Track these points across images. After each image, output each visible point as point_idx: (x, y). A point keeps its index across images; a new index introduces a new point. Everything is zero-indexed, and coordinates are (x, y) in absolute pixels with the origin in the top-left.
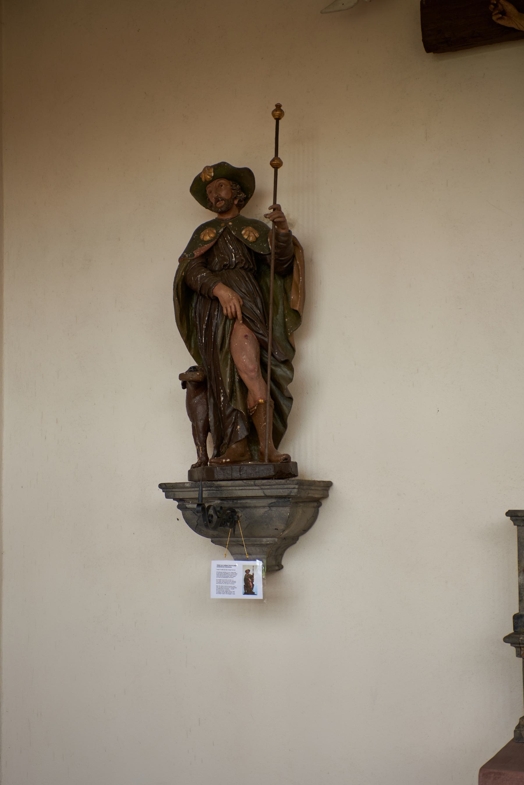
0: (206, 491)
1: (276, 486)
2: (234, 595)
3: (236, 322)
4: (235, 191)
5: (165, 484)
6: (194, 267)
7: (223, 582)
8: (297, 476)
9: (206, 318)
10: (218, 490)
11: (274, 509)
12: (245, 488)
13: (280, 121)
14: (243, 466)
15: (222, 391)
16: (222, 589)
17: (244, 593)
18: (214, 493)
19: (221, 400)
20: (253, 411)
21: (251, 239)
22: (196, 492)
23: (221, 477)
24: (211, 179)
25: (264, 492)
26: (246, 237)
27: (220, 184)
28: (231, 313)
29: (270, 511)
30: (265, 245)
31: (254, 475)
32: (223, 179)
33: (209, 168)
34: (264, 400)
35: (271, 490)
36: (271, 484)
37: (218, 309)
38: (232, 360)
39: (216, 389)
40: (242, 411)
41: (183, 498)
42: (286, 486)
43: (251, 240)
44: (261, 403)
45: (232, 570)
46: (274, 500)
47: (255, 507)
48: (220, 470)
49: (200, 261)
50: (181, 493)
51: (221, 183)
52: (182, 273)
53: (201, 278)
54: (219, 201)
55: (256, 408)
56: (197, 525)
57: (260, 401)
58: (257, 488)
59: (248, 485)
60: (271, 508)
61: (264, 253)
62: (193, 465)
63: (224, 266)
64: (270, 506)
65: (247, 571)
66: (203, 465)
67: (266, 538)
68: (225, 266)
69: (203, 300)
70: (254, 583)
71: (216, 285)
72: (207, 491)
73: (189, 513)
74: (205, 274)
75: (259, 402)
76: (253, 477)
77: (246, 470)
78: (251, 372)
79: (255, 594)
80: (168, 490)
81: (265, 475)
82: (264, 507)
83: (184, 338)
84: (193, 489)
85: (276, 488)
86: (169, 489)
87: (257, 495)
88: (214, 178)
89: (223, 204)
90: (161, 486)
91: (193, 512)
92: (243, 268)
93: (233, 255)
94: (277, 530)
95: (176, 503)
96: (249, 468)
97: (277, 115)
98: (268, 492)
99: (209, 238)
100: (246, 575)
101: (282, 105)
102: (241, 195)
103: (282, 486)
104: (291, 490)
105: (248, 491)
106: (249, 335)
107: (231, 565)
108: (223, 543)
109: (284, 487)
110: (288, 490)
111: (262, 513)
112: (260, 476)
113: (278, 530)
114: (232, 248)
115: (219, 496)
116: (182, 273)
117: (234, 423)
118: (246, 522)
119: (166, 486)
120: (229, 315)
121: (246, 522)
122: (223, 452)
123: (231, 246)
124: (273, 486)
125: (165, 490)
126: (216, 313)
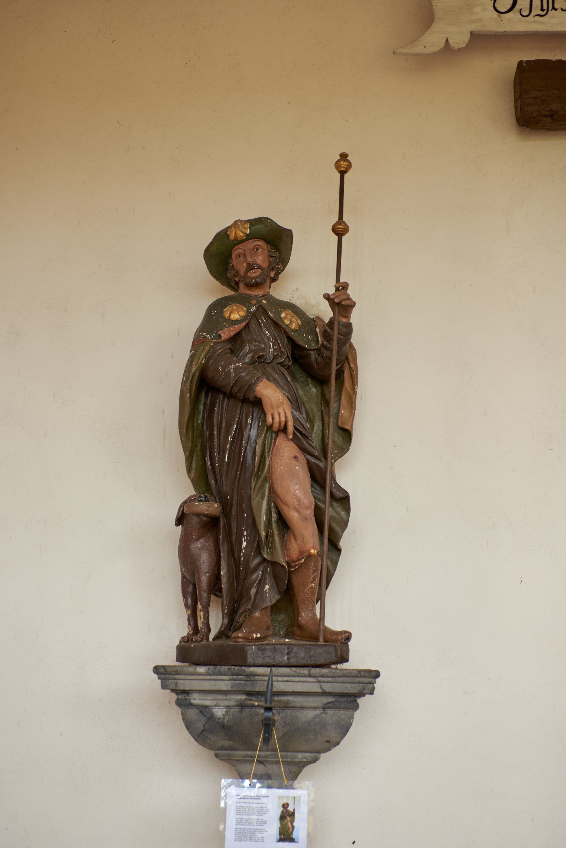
0: (230, 680)
1: (342, 679)
2: (262, 842)
3: (279, 436)
4: (273, 259)
5: (163, 667)
6: (220, 353)
7: (246, 822)
8: (347, 661)
9: (233, 426)
10: (248, 679)
11: (330, 712)
12: (294, 679)
13: (346, 176)
14: (292, 646)
15: (245, 533)
16: (244, 834)
17: (278, 840)
18: (241, 684)
19: (241, 547)
20: (296, 565)
21: (294, 326)
22: (213, 681)
23: (259, 661)
24: (244, 238)
25: (321, 686)
26: (287, 322)
27: (255, 246)
28: (279, 423)
29: (323, 715)
30: (310, 337)
31: (307, 660)
32: (260, 240)
33: (243, 222)
34: (317, 551)
35: (334, 684)
36: (336, 675)
37: (253, 415)
38: (272, 490)
39: (235, 529)
40: (285, 565)
41: (190, 689)
42: (356, 680)
43: (294, 327)
44: (313, 555)
45: (261, 803)
46: (330, 699)
47: (302, 708)
48: (257, 650)
49: (228, 347)
50: (187, 682)
51: (257, 245)
52: (202, 360)
53: (236, 369)
54: (253, 268)
55: (303, 561)
56: (203, 731)
57: (312, 551)
58: (312, 679)
59: (299, 675)
60: (325, 710)
61: (309, 348)
62: (183, 638)
63: (258, 357)
64: (325, 707)
65: (285, 806)
66: (205, 639)
67: (304, 754)
68: (260, 357)
69: (226, 400)
70: (294, 824)
71: (261, 381)
72: (230, 682)
73: (192, 713)
74: (240, 364)
75: (310, 552)
76: (306, 663)
77: (296, 653)
78: (307, 509)
79: (296, 840)
80: (167, 676)
81: (323, 661)
82: (315, 708)
83: (187, 453)
84: (209, 677)
85: (342, 682)
86: (169, 676)
87: (311, 691)
88: (249, 237)
89: (258, 274)
90: (157, 670)
91: (201, 711)
92: (281, 364)
93: (271, 344)
94: (328, 743)
95: (174, 696)
96: (300, 649)
97: (344, 166)
98: (328, 687)
99: (239, 317)
100: (283, 810)
101: (348, 155)
102: (280, 266)
103: (351, 678)
104: (364, 686)
105: (296, 683)
106: (299, 457)
107: (259, 796)
108: (232, 758)
109: (354, 680)
110: (360, 686)
111: (310, 717)
112: (316, 662)
113: (329, 742)
114: (269, 334)
115: (248, 689)
116: (202, 360)
117: (261, 580)
118: (284, 729)
119: (166, 670)
120: (276, 426)
121: (284, 729)
122: (240, 622)
123: (267, 332)
124: (337, 679)
125: (163, 676)
126: (249, 421)
